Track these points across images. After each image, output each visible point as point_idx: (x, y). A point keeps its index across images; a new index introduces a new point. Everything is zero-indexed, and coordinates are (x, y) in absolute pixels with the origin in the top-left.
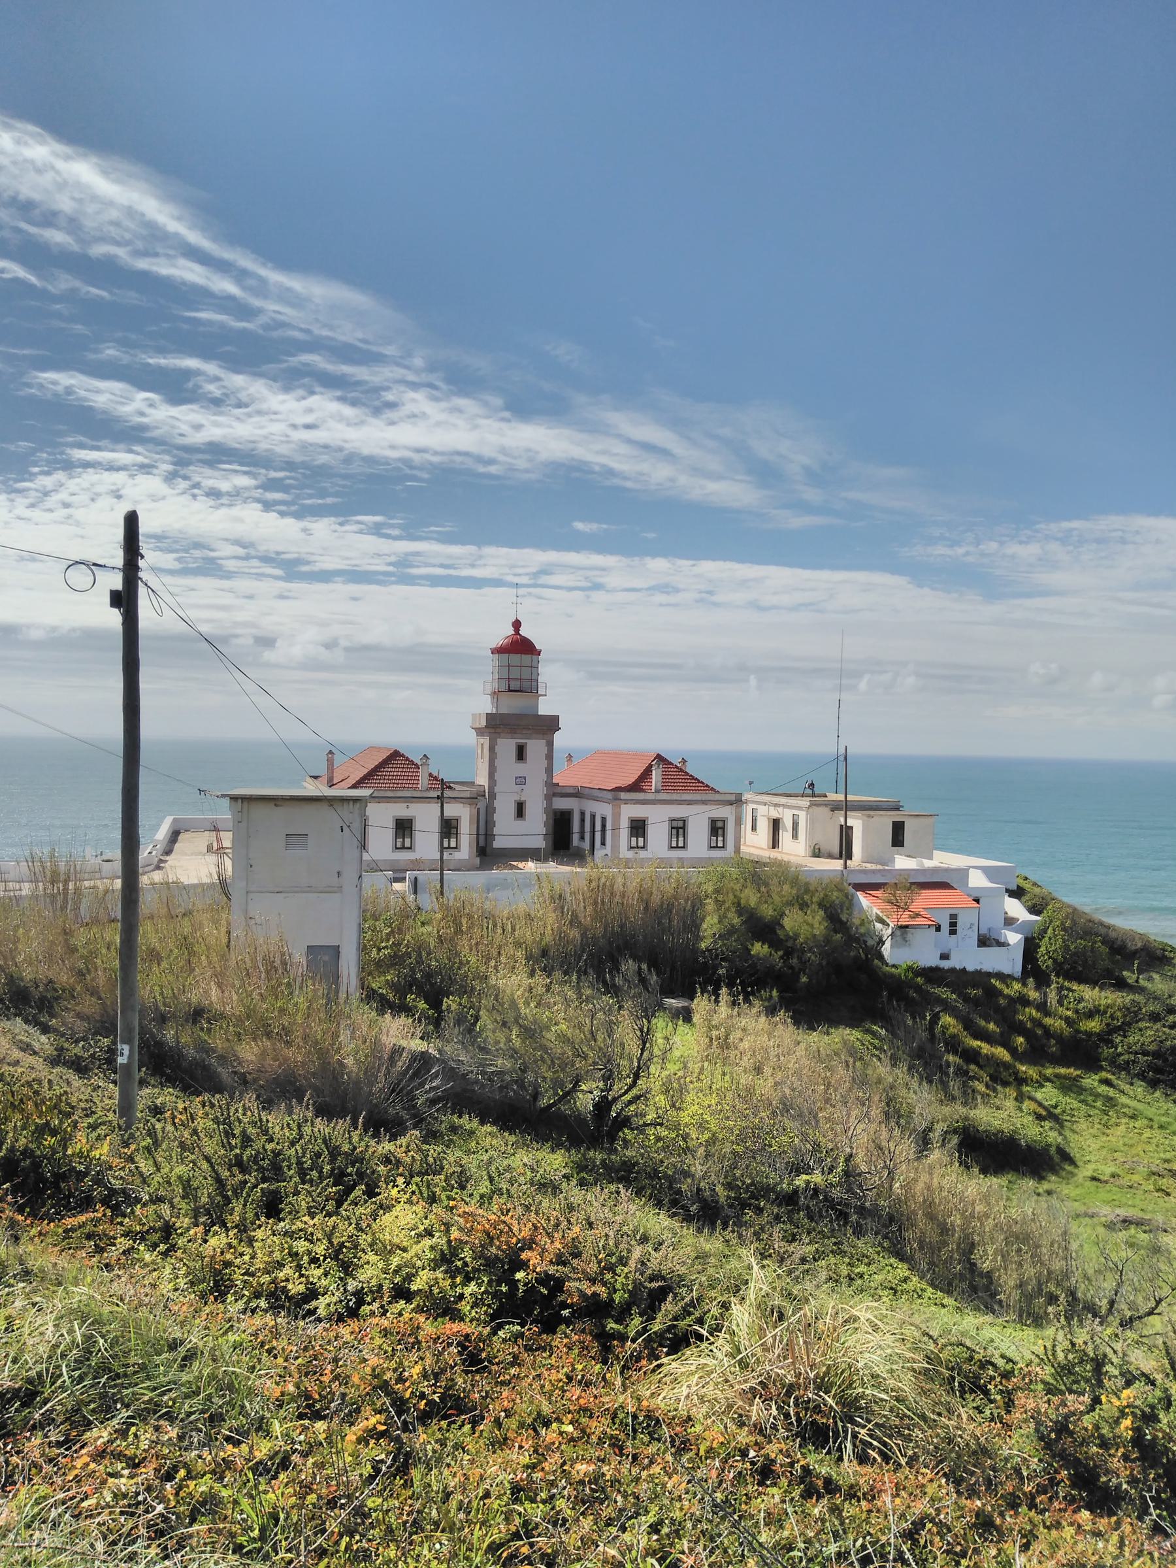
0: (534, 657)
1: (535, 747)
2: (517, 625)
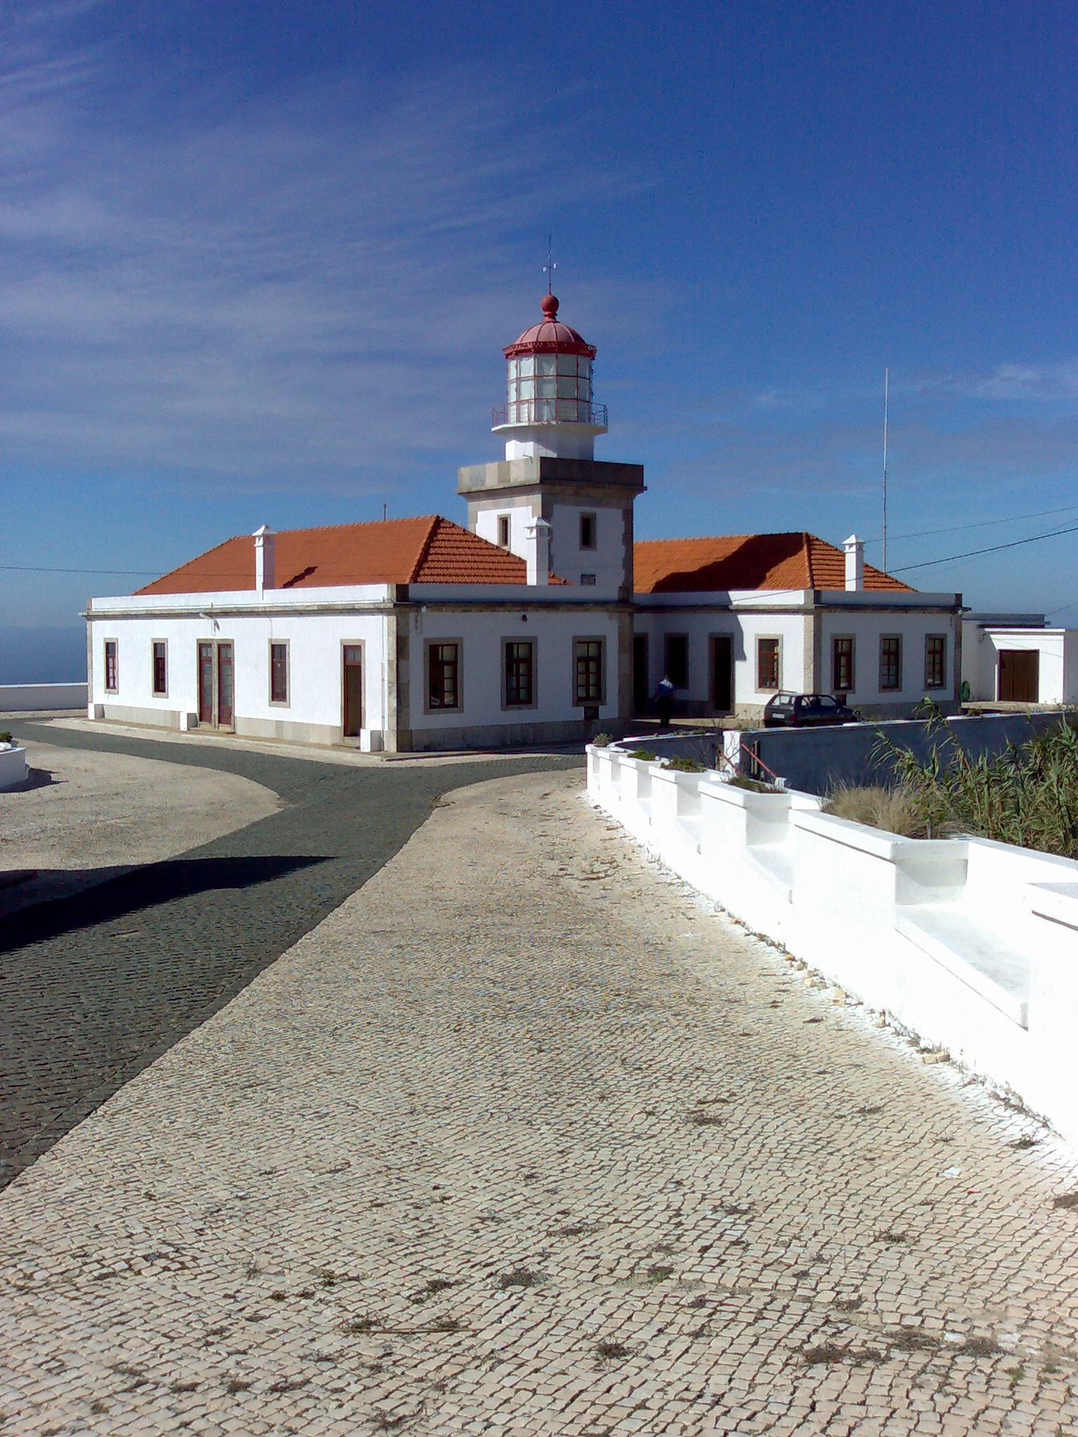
0: (583, 360)
1: (608, 521)
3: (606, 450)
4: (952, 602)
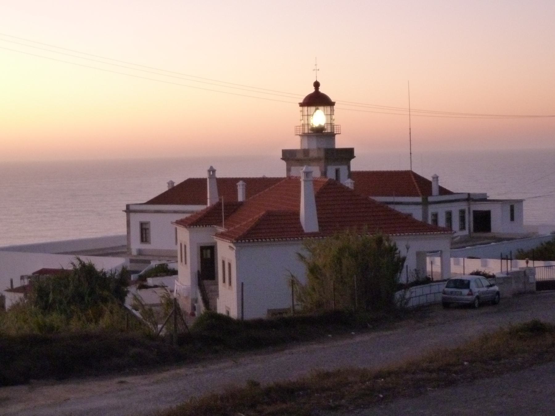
2: (317, 85)
3: (340, 143)
4: (466, 197)
